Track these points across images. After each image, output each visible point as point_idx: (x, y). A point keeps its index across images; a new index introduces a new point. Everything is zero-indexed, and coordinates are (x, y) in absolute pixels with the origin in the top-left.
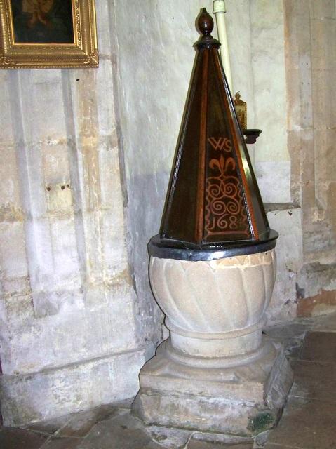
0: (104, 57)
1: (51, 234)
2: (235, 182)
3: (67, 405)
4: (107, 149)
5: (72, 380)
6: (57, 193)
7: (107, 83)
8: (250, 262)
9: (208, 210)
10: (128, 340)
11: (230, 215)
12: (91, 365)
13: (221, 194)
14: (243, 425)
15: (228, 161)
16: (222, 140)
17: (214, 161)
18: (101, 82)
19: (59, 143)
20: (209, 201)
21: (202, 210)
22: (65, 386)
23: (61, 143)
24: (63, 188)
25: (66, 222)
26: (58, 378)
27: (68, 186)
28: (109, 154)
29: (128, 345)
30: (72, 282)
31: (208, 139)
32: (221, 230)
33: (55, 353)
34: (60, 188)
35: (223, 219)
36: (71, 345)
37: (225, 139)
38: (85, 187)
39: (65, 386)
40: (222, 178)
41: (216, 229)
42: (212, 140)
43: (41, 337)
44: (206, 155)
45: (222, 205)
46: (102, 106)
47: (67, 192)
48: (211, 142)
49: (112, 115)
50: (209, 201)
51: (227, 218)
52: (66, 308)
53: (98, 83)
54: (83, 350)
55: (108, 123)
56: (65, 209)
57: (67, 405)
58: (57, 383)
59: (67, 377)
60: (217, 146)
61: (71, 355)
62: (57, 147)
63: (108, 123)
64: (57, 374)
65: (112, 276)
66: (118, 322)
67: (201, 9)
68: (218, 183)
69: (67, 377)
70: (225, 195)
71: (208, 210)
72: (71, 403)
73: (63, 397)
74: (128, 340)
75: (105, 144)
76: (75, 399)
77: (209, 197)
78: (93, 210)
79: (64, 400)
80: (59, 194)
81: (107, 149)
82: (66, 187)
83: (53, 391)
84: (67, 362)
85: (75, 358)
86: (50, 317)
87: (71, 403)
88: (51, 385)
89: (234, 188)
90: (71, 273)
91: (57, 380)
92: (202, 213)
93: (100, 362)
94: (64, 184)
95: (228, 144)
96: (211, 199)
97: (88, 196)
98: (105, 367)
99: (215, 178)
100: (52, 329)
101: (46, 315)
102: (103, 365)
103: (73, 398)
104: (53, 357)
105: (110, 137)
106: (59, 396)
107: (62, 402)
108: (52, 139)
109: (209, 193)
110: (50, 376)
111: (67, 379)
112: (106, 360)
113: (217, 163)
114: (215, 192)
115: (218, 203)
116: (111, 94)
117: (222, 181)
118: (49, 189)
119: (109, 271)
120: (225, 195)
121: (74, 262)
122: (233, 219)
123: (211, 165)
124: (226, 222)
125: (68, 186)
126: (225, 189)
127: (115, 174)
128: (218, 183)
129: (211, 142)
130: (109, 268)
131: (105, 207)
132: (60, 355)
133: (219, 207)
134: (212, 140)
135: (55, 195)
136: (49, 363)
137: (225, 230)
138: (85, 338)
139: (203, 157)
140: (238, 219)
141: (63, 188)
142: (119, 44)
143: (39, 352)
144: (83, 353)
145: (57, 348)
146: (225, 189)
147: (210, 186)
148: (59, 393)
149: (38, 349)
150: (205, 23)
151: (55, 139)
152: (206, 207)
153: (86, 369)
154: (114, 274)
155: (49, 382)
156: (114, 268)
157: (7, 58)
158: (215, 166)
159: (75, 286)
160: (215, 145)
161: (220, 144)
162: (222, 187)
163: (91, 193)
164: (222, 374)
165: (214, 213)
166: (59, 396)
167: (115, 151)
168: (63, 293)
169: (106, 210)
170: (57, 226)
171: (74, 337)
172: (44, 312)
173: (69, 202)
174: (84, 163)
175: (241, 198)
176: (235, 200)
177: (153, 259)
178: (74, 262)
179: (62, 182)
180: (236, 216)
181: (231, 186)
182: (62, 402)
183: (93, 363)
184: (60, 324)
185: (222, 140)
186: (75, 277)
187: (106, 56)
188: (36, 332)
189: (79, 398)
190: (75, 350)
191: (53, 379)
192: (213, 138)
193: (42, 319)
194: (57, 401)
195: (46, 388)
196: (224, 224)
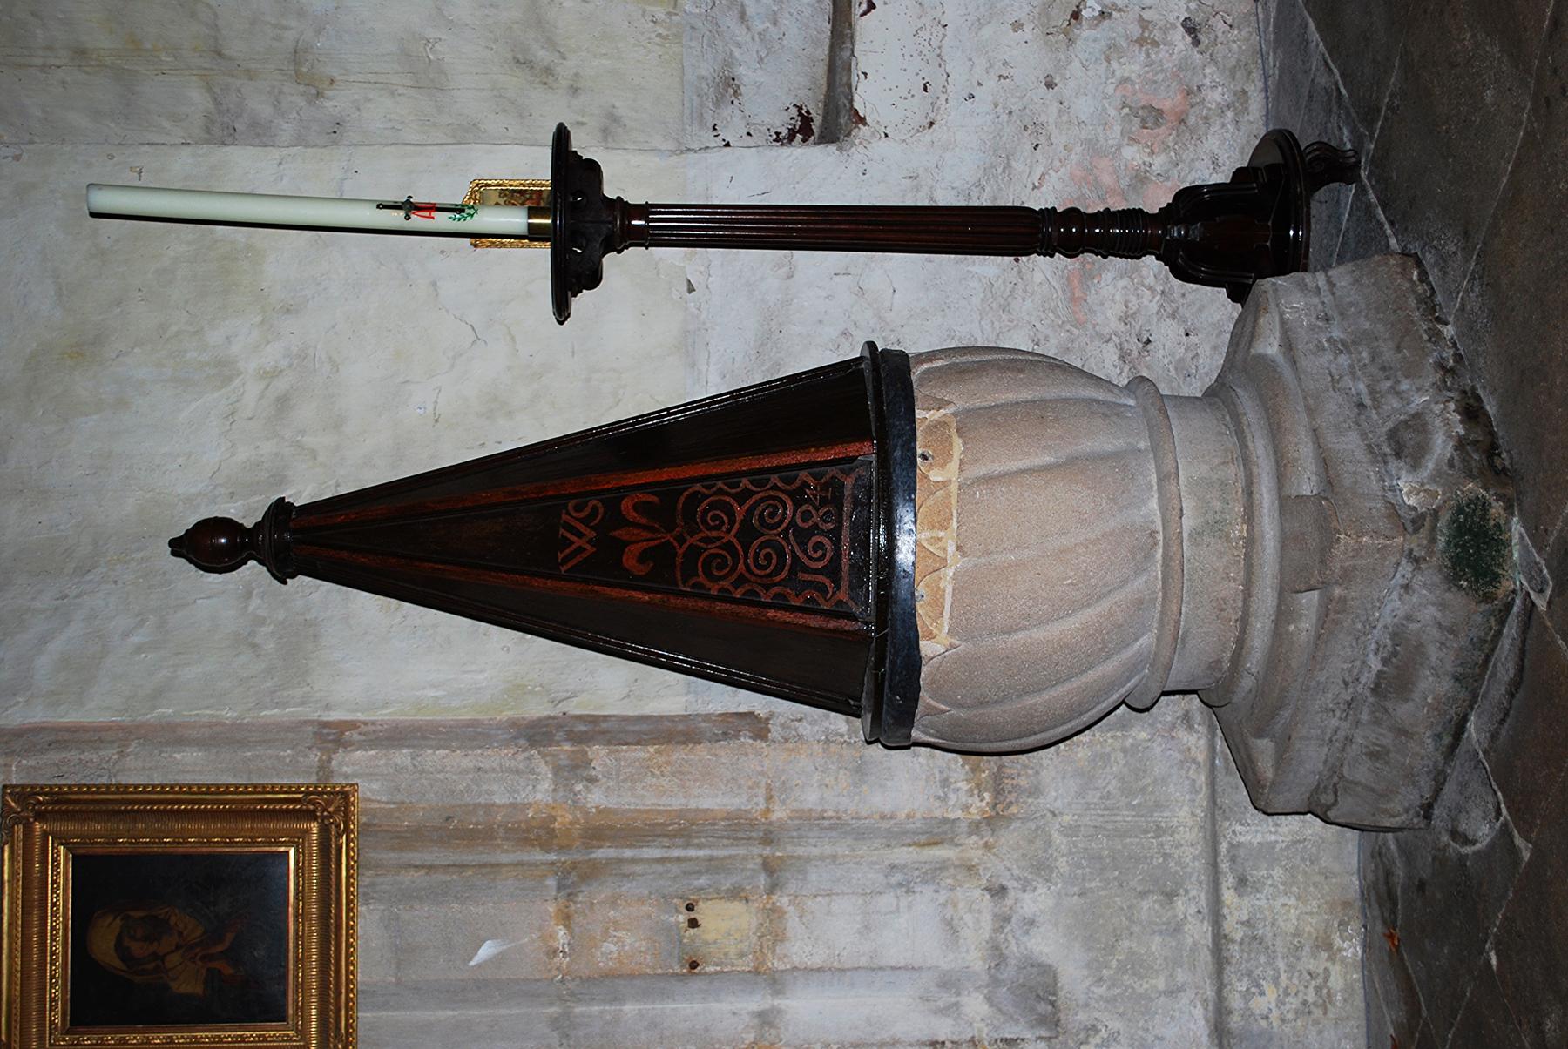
0: (324, 767)
1: (819, 970)
2: (695, 499)
3: (1336, 982)
4: (592, 780)
5: (1263, 959)
6: (707, 943)
7: (399, 769)
8: (942, 534)
9: (775, 590)
10: (1178, 756)
11: (793, 523)
12: (1228, 895)
13: (729, 547)
14: (1460, 603)
15: (632, 515)
16: (568, 527)
17: (629, 560)
18: (397, 789)
19: (567, 926)
20: (747, 587)
21: (771, 613)
22: (1276, 981)
23: (566, 919)
24: (693, 923)
25: (793, 923)
26: (1247, 1001)
27: (690, 908)
28: (607, 775)
29: (1194, 761)
30: (968, 918)
31: (563, 569)
32: (838, 554)
33: (1173, 992)
34: (692, 931)
35: (803, 545)
36: (1157, 939)
37: (564, 517)
38: (700, 847)
39: (1276, 981)
40: (682, 540)
41: (833, 570)
42: (566, 560)
43: (1115, 1025)
44: (609, 585)
45: (762, 546)
46: (468, 788)
47: (704, 912)
48: (570, 565)
49: (497, 757)
50: (747, 587)
51: (803, 536)
52: (1046, 945)
53: (399, 798)
54: (1179, 903)
55: (517, 772)
56: (755, 922)
57: (1336, 982)
58: (1260, 1004)
59: (1249, 974)
60: (583, 542)
61: (1190, 940)
62: (577, 930)
63: (517, 772)
64: (1235, 1002)
65: (970, 793)
66: (1113, 787)
67: (174, 554)
68: (694, 552)
69: (1249, 974)
70: (731, 537)
71: (775, 590)
72: (1336, 970)
73: (1311, 990)
74: (1178, 756)
75: (579, 787)
76: (1324, 955)
77: (736, 585)
78: (767, 833)
79: (1318, 989)
80: (710, 937)
81: (592, 780)
82: (692, 915)
83: (1283, 1021)
84: (1205, 957)
85: (1198, 932)
86: (1061, 994)
87: (1336, 970)
88: (1264, 1023)
89: (713, 506)
90: (944, 919)
91: (1252, 1004)
92: (781, 615)
93: (1225, 866)
94: (682, 918)
95: (578, 508)
96: (741, 580)
97: (725, 842)
98: (1242, 852)
99: (679, 560)
100: (1101, 990)
101: (1052, 1003)
102: (1233, 860)
103: (1319, 963)
104: (1184, 999)
105: (557, 770)
106: (1305, 1003)
107: (1325, 1001)
108: (556, 945)
109: (725, 584)
110: (1235, 1022)
111: (1258, 972)
112: (1224, 847)
113: (635, 549)
114: (720, 568)
115: (756, 555)
116: (433, 757)
117: (690, 540)
118: (694, 965)
119: (953, 798)
120: (731, 537)
121: (909, 907)
122: (806, 516)
123: (642, 570)
124: (815, 539)
125: (690, 908)
126: (715, 534)
127: (668, 763)
128: (694, 552)
129: (570, 565)
130: (943, 799)
131: (761, 800)
132: (1181, 976)
133: (768, 557)
134: (566, 560)
135: (712, 948)
136: (1199, 1012)
137: (837, 544)
138: (1143, 895)
139: (615, 593)
140: (808, 501)
141: (693, 923)
142: (285, 705)
143: (1161, 1039)
144: (1190, 905)
145: (1161, 983)
146: (715, 534)
147: (702, 579)
148: (1293, 1003)
149: (1150, 1038)
150: (210, 546)
151: (553, 936)
152: (765, 598)
153: (1236, 908)
154: (964, 786)
155: (1255, 1028)
156: (945, 783)
157: (314, 812)
158: (642, 559)
159: (979, 912)
160: (581, 550)
161: (580, 535)
162: (708, 540)
163: (719, 834)
164: (1292, 628)
165: (784, 575)
166: (1305, 1003)
167: (599, 755)
168: (996, 948)
169: (769, 798)
170: (799, 949)
171: (1136, 929)
172: (1043, 1008)
173: (737, 907)
174: (631, 846)
175: (745, 482)
176: (749, 502)
177: (916, 734)
178: (909, 907)
179: (678, 923)
180: (797, 505)
181: (705, 511)
182: (1325, 1001)
183: (1224, 886)
184: (1088, 966)
185: (568, 527)
186: (955, 905)
187: (321, 768)
188: (1098, 1040)
189: (1324, 945)
190: (1177, 929)
191: (1248, 1014)
192: (561, 556)
193: (1062, 1016)
194: (1318, 1013)
195: (1271, 1039)
196: (818, 546)
